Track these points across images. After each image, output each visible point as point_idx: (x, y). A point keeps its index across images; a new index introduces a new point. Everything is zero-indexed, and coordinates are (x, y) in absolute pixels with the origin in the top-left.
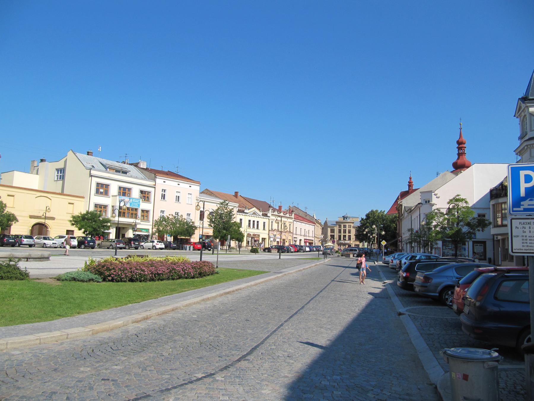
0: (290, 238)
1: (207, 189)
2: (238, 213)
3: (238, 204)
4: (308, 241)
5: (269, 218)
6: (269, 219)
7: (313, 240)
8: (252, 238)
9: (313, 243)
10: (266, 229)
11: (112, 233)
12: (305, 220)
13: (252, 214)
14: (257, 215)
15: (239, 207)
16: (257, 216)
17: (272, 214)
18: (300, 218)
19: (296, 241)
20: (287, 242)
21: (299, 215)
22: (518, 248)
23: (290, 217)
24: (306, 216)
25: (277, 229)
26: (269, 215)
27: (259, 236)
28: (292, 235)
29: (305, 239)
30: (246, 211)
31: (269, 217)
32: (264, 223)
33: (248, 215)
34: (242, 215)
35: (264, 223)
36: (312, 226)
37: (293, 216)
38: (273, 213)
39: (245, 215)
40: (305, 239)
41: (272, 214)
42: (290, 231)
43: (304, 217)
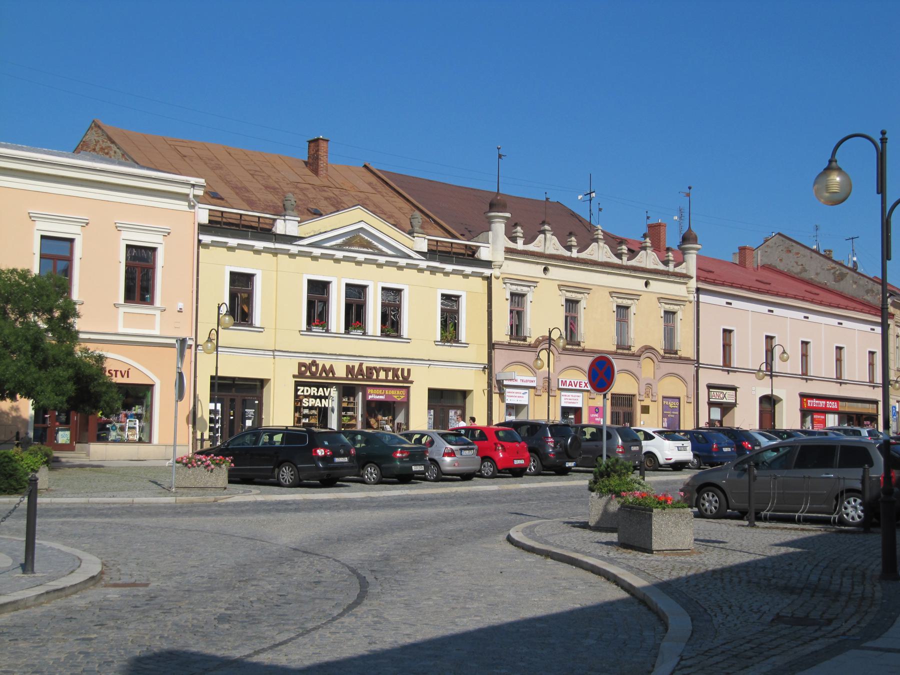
0: (671, 387)
1: (310, 142)
2: (206, 239)
3: (202, 181)
4: (832, 405)
5: (487, 272)
6: (489, 279)
7: (875, 402)
8: (347, 391)
9: (873, 418)
10: (463, 334)
11: (272, 381)
12: (823, 296)
13: (339, 248)
14: (382, 254)
15: (212, 196)
16: (382, 260)
17: (509, 251)
18: (779, 283)
19: (726, 408)
20: (645, 410)
21: (805, 276)
22: (439, 275)
23: (671, 268)
24: (841, 277)
25: (659, 345)
26: (484, 254)
27: (403, 380)
28: (688, 371)
29: (803, 396)
30: (281, 227)
31: (488, 264)
32: (450, 303)
33: (294, 249)
34: (266, 250)
35: (450, 303)
36: (867, 327)
37: (690, 265)
38: (520, 245)
39: (275, 252)
40: (803, 396)
41: (509, 251)
42: (671, 353)
43: (832, 284)
